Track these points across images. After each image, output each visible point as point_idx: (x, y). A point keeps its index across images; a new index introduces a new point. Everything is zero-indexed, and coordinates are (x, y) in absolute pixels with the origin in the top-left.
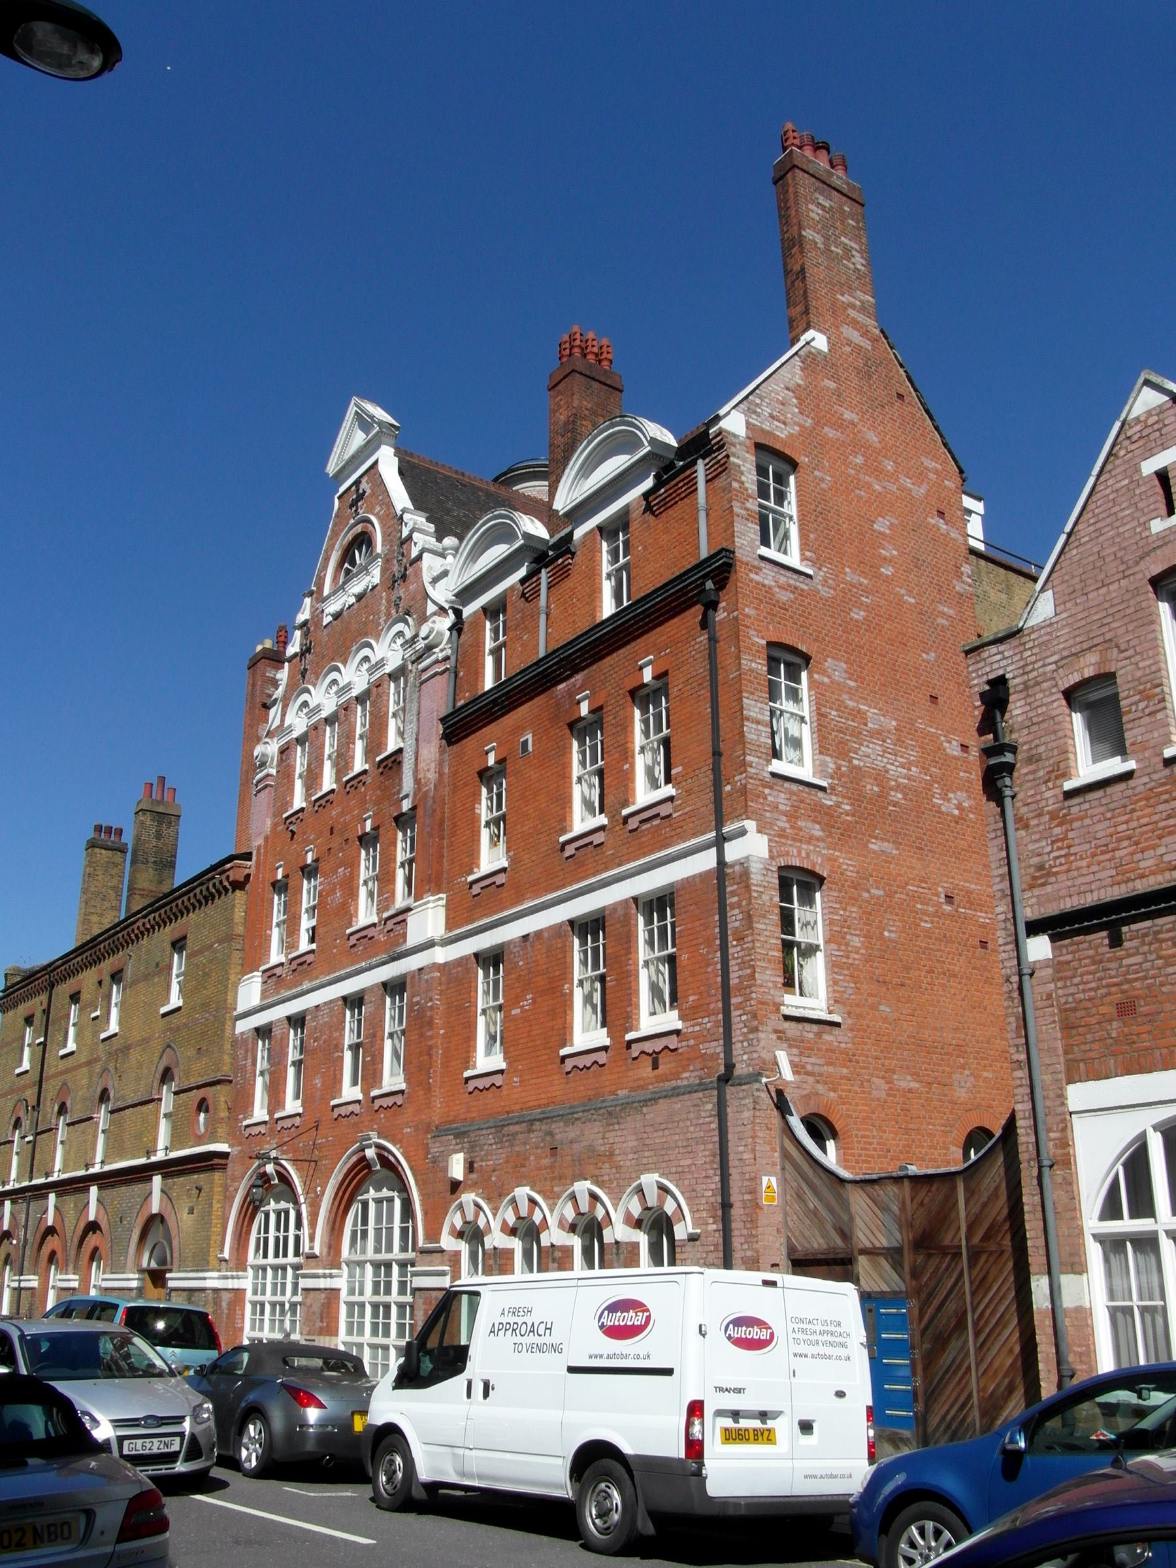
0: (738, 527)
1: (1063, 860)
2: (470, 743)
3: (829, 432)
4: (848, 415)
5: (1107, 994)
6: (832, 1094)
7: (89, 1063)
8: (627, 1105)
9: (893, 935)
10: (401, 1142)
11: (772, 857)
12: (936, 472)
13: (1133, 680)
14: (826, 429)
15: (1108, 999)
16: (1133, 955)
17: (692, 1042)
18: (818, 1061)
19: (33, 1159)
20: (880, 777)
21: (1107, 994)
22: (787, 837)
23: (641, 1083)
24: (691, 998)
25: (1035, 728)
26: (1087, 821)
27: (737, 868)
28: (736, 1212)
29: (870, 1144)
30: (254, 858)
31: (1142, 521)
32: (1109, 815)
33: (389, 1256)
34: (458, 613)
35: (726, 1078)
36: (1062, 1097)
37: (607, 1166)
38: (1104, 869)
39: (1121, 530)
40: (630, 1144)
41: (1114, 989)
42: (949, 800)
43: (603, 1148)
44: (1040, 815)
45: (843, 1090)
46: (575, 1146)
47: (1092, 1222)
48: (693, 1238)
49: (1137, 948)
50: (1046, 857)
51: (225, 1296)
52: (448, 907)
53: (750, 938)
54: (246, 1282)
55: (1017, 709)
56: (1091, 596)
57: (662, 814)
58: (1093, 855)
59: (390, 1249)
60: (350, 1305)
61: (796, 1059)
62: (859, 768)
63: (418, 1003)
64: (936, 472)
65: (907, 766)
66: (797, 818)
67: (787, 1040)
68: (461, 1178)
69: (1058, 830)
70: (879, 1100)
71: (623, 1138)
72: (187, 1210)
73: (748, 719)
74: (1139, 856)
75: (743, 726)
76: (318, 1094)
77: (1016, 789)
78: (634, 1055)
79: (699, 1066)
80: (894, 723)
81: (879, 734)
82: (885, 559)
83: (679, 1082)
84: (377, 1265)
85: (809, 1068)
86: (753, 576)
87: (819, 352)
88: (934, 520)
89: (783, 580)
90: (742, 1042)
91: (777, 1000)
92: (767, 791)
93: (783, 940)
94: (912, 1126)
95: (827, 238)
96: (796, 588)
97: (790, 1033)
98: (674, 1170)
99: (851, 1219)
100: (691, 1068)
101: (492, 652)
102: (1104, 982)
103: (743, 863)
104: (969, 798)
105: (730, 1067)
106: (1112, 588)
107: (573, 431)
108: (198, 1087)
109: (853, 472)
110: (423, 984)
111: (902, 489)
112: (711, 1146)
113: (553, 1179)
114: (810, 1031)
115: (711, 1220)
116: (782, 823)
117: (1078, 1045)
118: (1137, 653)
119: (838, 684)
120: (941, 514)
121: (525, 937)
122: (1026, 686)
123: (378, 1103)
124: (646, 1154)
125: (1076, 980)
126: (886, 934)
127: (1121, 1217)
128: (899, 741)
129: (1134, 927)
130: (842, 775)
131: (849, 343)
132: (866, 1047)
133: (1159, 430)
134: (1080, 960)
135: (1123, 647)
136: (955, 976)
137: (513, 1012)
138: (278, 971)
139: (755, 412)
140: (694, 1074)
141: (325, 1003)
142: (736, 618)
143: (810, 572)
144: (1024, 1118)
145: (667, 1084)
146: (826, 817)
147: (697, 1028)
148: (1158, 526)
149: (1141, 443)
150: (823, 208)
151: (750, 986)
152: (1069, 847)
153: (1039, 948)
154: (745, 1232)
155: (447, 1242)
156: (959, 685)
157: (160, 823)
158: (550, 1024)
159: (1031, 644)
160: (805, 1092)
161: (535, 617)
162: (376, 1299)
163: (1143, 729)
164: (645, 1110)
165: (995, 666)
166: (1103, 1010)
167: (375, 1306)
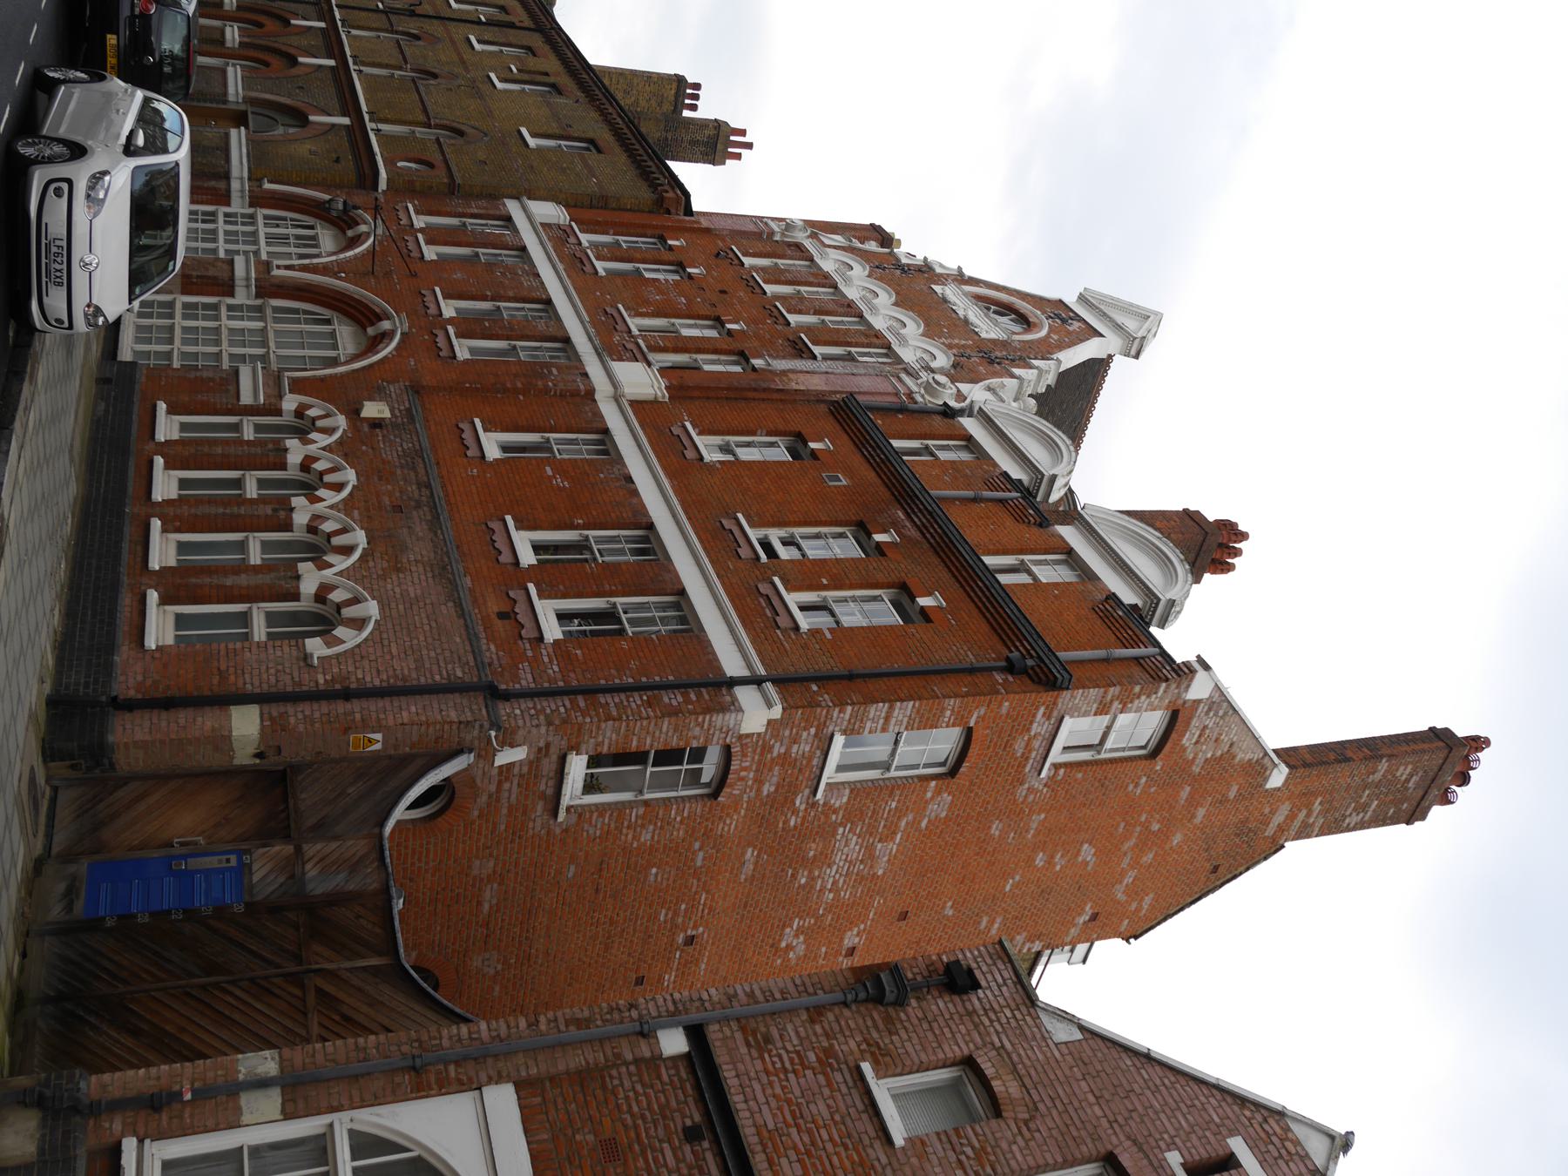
0: (1093, 692)
1: (778, 1065)
2: (830, 424)
3: (1185, 792)
4: (1201, 812)
5: (625, 1126)
6: (476, 813)
7: (463, 62)
8: (453, 585)
9: (652, 878)
11: (740, 737)
12: (1138, 910)
13: (996, 1140)
14: (1188, 789)
15: (619, 1124)
16: (675, 1156)
17: (530, 653)
18: (513, 797)
19: (360, 9)
20: (825, 859)
21: (625, 1126)
22: (762, 754)
25: (925, 1026)
26: (826, 1092)
27: (728, 698)
28: (341, 707)
29: (420, 860)
31: (1177, 1140)
32: (837, 1117)
33: (272, 345)
34: (961, 412)
35: (494, 694)
36: (498, 1079)
37: (385, 565)
38: (774, 1116)
39: (1162, 1116)
40: (411, 590)
41: (633, 1134)
42: (796, 936)
44: (827, 1035)
45: (480, 826)
47: (343, 1124)
48: (306, 657)
49: (684, 1160)
50: (779, 1045)
51: (221, 185)
52: (654, 403)
54: (238, 206)
55: (942, 1005)
56: (1083, 1083)
58: (789, 1102)
60: (215, 307)
61: (516, 770)
62: (834, 833)
63: (550, 372)
64: (1138, 910)
65: (835, 888)
66: (782, 765)
67: (538, 760)
68: (364, 414)
69: (812, 1057)
70: (470, 867)
71: (416, 582)
73: (891, 708)
74: (794, 1157)
77: (854, 1007)
80: (880, 872)
81: (870, 856)
82: (1052, 857)
84: (264, 331)
85: (506, 786)
86: (1042, 710)
87: (1266, 779)
88: (1089, 910)
89: (1036, 744)
91: (583, 747)
92: (813, 731)
93: (647, 753)
94: (440, 906)
95: (1378, 785)
96: (1027, 759)
97: (545, 762)
99: (336, 838)
101: (927, 447)
102: (640, 1122)
103: (734, 706)
104: (798, 958)
105: (507, 696)
106: (1096, 1108)
108: (446, 161)
109: (1143, 819)
111: (1123, 874)
112: (414, 675)
113: (368, 510)
114: (545, 786)
116: (778, 749)
117: (562, 1094)
118: (1027, 1142)
119: (925, 809)
120: (1094, 917)
121: (629, 479)
122: (972, 1013)
123: (440, 333)
124: (401, 607)
125: (639, 1087)
126: (654, 870)
127: (354, 1159)
128: (861, 878)
129: (709, 1156)
130: (827, 816)
131: (1273, 812)
132: (528, 851)
133: (1281, 1156)
134: (663, 1091)
135: (1032, 1125)
138: (572, 240)
139: (1210, 709)
142: (998, 692)
143: (1043, 775)
144: (470, 1033)
146: (786, 792)
147: (546, 659)
148: (1174, 1159)
149: (1263, 1135)
150: (1407, 781)
151: (598, 714)
152: (794, 1071)
153: (674, 1042)
154: (317, 715)
155: (290, 403)
156: (918, 943)
159: (1019, 1016)
161: (968, 487)
163: (941, 1154)
164: (450, 604)
165: (989, 977)
166: (607, 1121)
167: (217, 330)
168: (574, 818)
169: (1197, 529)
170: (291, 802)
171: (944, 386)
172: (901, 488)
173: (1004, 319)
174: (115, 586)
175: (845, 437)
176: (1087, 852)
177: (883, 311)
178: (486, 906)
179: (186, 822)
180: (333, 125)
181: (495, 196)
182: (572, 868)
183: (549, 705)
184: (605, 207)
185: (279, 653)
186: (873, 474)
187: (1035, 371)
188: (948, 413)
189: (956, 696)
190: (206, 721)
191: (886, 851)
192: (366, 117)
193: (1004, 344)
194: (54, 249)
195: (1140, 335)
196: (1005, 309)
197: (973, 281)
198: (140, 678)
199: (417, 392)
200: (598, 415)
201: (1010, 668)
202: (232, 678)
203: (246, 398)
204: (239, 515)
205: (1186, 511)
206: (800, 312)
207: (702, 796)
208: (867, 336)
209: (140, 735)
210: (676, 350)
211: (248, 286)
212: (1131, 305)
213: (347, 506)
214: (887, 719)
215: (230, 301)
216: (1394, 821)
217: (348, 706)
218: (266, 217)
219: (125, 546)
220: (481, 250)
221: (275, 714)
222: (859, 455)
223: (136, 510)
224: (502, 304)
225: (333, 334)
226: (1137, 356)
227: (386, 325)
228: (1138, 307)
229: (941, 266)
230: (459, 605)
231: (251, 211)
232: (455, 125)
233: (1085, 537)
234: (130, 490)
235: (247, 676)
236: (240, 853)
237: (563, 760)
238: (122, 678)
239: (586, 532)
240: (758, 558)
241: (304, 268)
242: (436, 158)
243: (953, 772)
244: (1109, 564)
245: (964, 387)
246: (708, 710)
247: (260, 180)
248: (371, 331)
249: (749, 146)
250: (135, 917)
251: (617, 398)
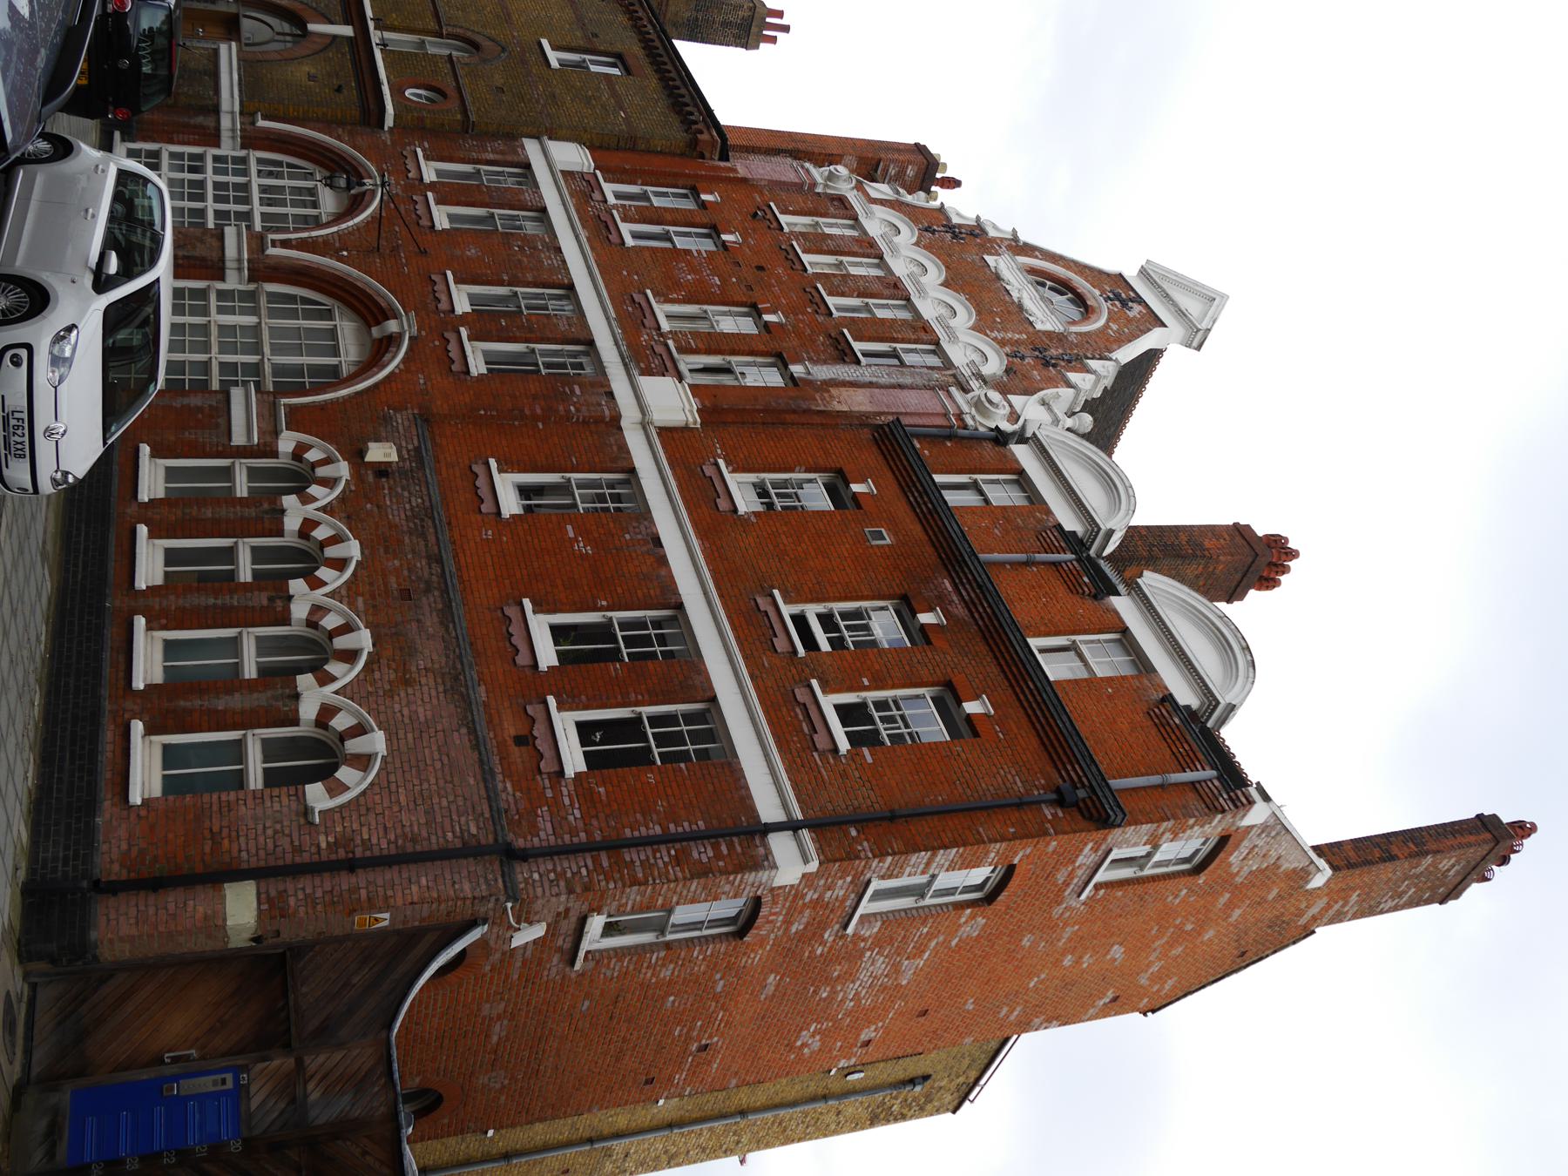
0: (1146, 827)
2: (872, 458)
4: (1237, 913)
6: (488, 968)
8: (466, 702)
10: (407, 370)
11: (772, 889)
14: (1227, 895)
17: (549, 794)
20: (850, 976)
23: (496, 721)
24: (602, 790)
27: (761, 850)
28: (345, 881)
30: (722, 164)
33: (267, 350)
35: (511, 856)
37: (393, 676)
40: (421, 710)
43: (414, 669)
46: (414, 625)
48: (307, 811)
52: (685, 429)
53: (680, 875)
54: (228, 148)
57: (816, 737)
59: (276, 350)
62: (862, 955)
63: (572, 391)
68: (369, 458)
71: (426, 701)
72: (313, 71)
73: (934, 855)
75: (926, 850)
76: (458, 253)
78: (529, 708)
79: (521, 806)
81: (896, 969)
83: (500, 777)
86: (1090, 845)
88: (1110, 994)
90: (554, 870)
91: (605, 910)
92: (849, 879)
95: (1418, 877)
98: (392, 778)
100: (518, 794)
103: (766, 861)
105: (524, 856)
107: (1195, 556)
110: (593, 399)
111: (1148, 966)
113: (373, 597)
115: (331, 839)
116: (811, 895)
120: (1115, 999)
121: (657, 542)
124: (410, 736)
128: (884, 988)
130: (855, 944)
136: (617, 1060)
137: (569, 528)
140: (511, 799)
141: (564, 262)
143: (1083, 897)
145: (496, 759)
146: (813, 933)
147: (567, 801)
151: (622, 878)
154: (319, 894)
157: (739, 26)
158: (559, 582)
160: (492, 943)
162: (214, 331)
164: (464, 731)
167: (205, 329)
168: (592, 964)
169: (1247, 550)
170: (292, 997)
171: (997, 406)
172: (946, 547)
173: (1057, 298)
174: (95, 718)
175: (889, 475)
176: (1117, 952)
177: (934, 298)
178: (495, 1039)
179: (177, 1025)
180: (335, 37)
181: (512, 137)
182: (587, 1003)
183: (568, 865)
184: (633, 150)
185: (277, 806)
186: (919, 528)
187: (1093, 377)
188: (1000, 439)
189: (1003, 839)
190: (197, 904)
191: (910, 969)
192: (371, 25)
193: (1058, 338)
194: (13, 422)
195: (1203, 326)
196: (1063, 287)
197: (1028, 250)
198: (124, 846)
199: (427, 420)
200: (624, 449)
201: (1060, 802)
202: (226, 842)
203: (238, 439)
204: (232, 607)
205: (1236, 525)
206: (843, 295)
207: (726, 934)
208: (915, 329)
209: (126, 929)
210: (709, 352)
211: (240, 269)
212: (1196, 283)
213: (348, 593)
214: (928, 864)
215: (220, 286)
216: (1428, 902)
217: (353, 879)
218: (260, 161)
219: (107, 655)
220: (497, 211)
221: (273, 893)
222: (903, 500)
223: (117, 603)
224: (520, 290)
225: (333, 333)
226: (1199, 348)
227: (392, 326)
228: (1203, 286)
229: (995, 227)
230: (473, 731)
231: (243, 153)
232: (469, 34)
233: (1142, 613)
234: (111, 572)
235: (242, 840)
236: (236, 1071)
237: (582, 922)
238: (105, 847)
239: (609, 614)
240: (795, 651)
241: (302, 245)
242: (448, 84)
243: (990, 898)
244: (1166, 650)
245: (1017, 400)
246: (741, 868)
247: (253, 114)
248: (376, 332)
249: (786, 29)
250: (122, 1162)
251: (644, 425)
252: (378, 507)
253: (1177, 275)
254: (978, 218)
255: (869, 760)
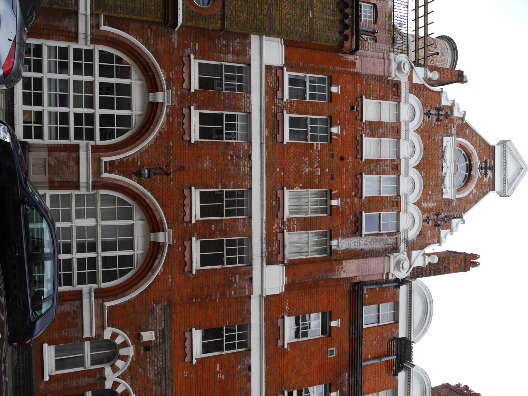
121: (249, 368)
222: (348, 329)
252: (144, 370)
253: (517, 152)
254: (454, 101)
255: (336, 191)
